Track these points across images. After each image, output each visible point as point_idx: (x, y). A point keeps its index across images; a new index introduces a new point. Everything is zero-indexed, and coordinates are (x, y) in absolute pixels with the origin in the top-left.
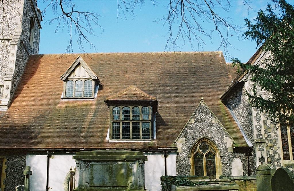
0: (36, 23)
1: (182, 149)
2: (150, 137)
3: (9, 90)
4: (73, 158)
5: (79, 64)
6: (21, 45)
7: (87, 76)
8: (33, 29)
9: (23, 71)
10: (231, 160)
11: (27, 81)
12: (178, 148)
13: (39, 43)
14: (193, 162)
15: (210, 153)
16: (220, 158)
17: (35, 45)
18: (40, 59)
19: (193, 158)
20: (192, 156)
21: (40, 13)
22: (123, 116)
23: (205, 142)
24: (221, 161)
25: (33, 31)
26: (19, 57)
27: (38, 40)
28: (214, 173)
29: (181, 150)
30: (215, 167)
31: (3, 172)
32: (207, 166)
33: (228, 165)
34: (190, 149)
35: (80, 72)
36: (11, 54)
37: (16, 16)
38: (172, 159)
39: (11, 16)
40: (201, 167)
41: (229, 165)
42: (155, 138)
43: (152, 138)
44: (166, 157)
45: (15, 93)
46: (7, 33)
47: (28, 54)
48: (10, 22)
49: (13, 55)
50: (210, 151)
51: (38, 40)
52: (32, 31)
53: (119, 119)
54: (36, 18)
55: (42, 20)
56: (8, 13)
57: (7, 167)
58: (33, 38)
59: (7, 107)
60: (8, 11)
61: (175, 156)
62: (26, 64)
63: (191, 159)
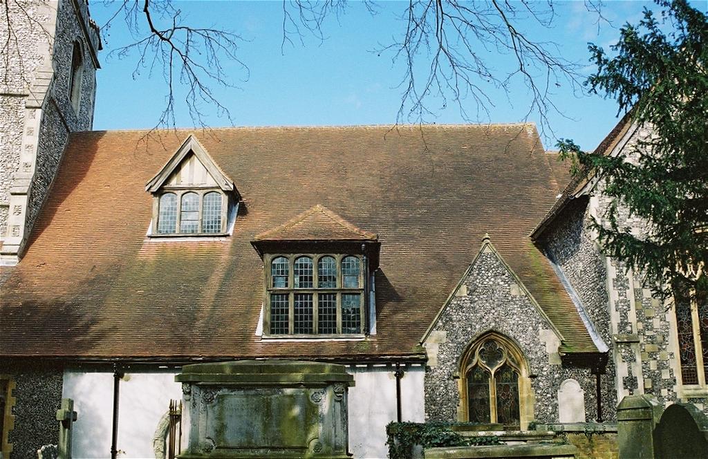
0: (87, 55)
1: (439, 359)
2: (362, 328)
3: (22, 217)
4: (177, 380)
5: (191, 154)
6: (50, 108)
7: (210, 183)
8: (79, 70)
9: (55, 170)
10: (555, 385)
11: (65, 194)
12: (429, 356)
13: (94, 103)
14: (464, 388)
15: (505, 368)
16: (529, 379)
17: (84, 109)
18: (97, 141)
19: (464, 381)
20: (462, 375)
21: (97, 30)
22: (297, 280)
23: (493, 341)
24: (532, 386)
25: (79, 73)
26: (45, 137)
27: (92, 96)
28: (516, 415)
29: (436, 361)
30: (517, 401)
31: (8, 412)
32: (498, 398)
33: (548, 395)
34: (457, 358)
35: (192, 172)
36: (25, 130)
37: (38, 38)
38: (414, 382)
39: (27, 38)
40: (485, 402)
41: (553, 397)
42: (373, 331)
43: (367, 332)
44: (399, 376)
45: (37, 224)
46: (18, 80)
47: (68, 130)
48: (23, 52)
49: (30, 132)
50: (505, 364)
51: (92, 96)
52: (77, 74)
53: (287, 285)
54: (86, 44)
55: (100, 48)
56: (20, 32)
57: (17, 402)
58: (81, 90)
59: (16, 257)
60: (20, 27)
61: (422, 374)
62: (63, 154)
63: (459, 381)
